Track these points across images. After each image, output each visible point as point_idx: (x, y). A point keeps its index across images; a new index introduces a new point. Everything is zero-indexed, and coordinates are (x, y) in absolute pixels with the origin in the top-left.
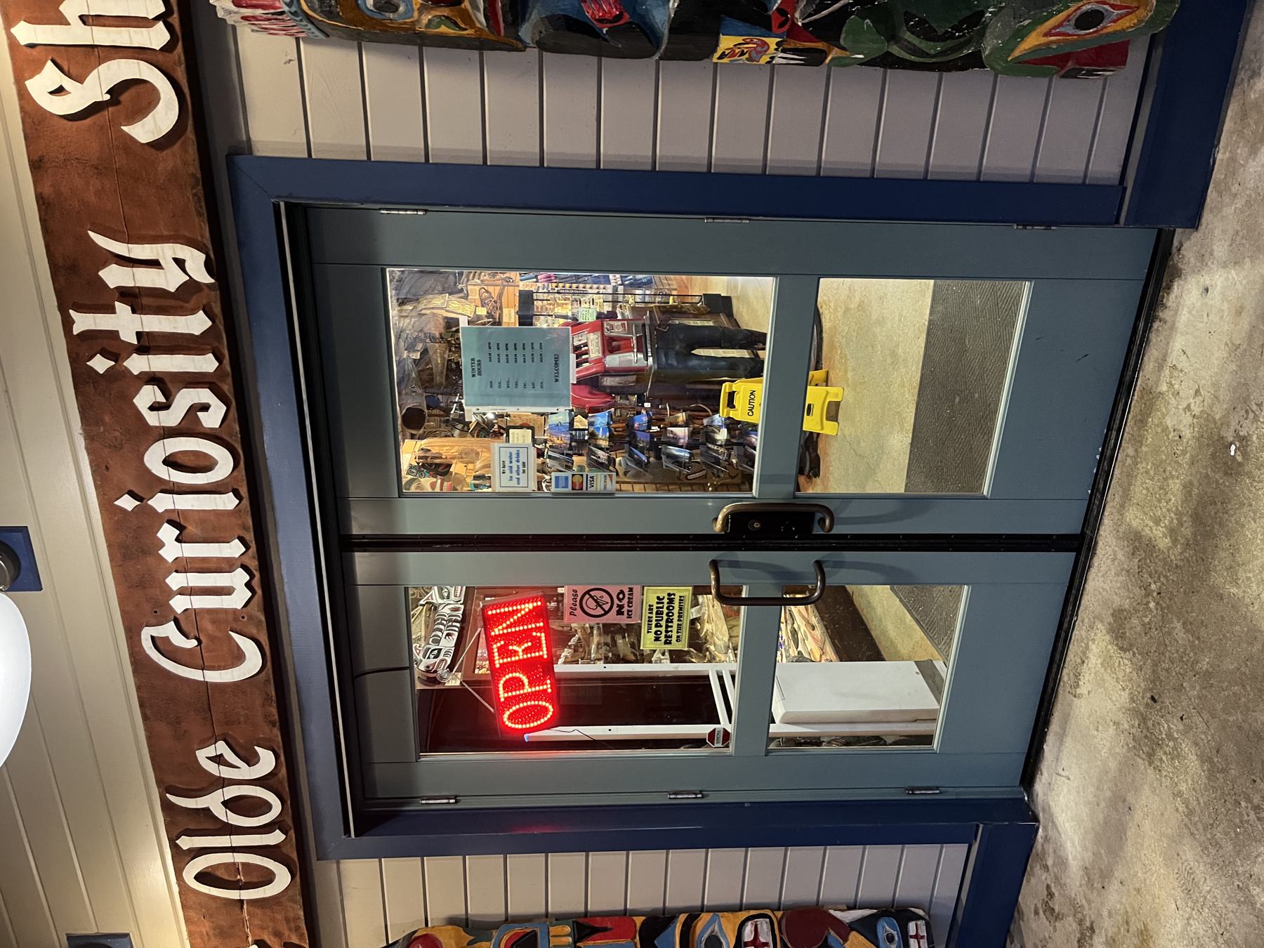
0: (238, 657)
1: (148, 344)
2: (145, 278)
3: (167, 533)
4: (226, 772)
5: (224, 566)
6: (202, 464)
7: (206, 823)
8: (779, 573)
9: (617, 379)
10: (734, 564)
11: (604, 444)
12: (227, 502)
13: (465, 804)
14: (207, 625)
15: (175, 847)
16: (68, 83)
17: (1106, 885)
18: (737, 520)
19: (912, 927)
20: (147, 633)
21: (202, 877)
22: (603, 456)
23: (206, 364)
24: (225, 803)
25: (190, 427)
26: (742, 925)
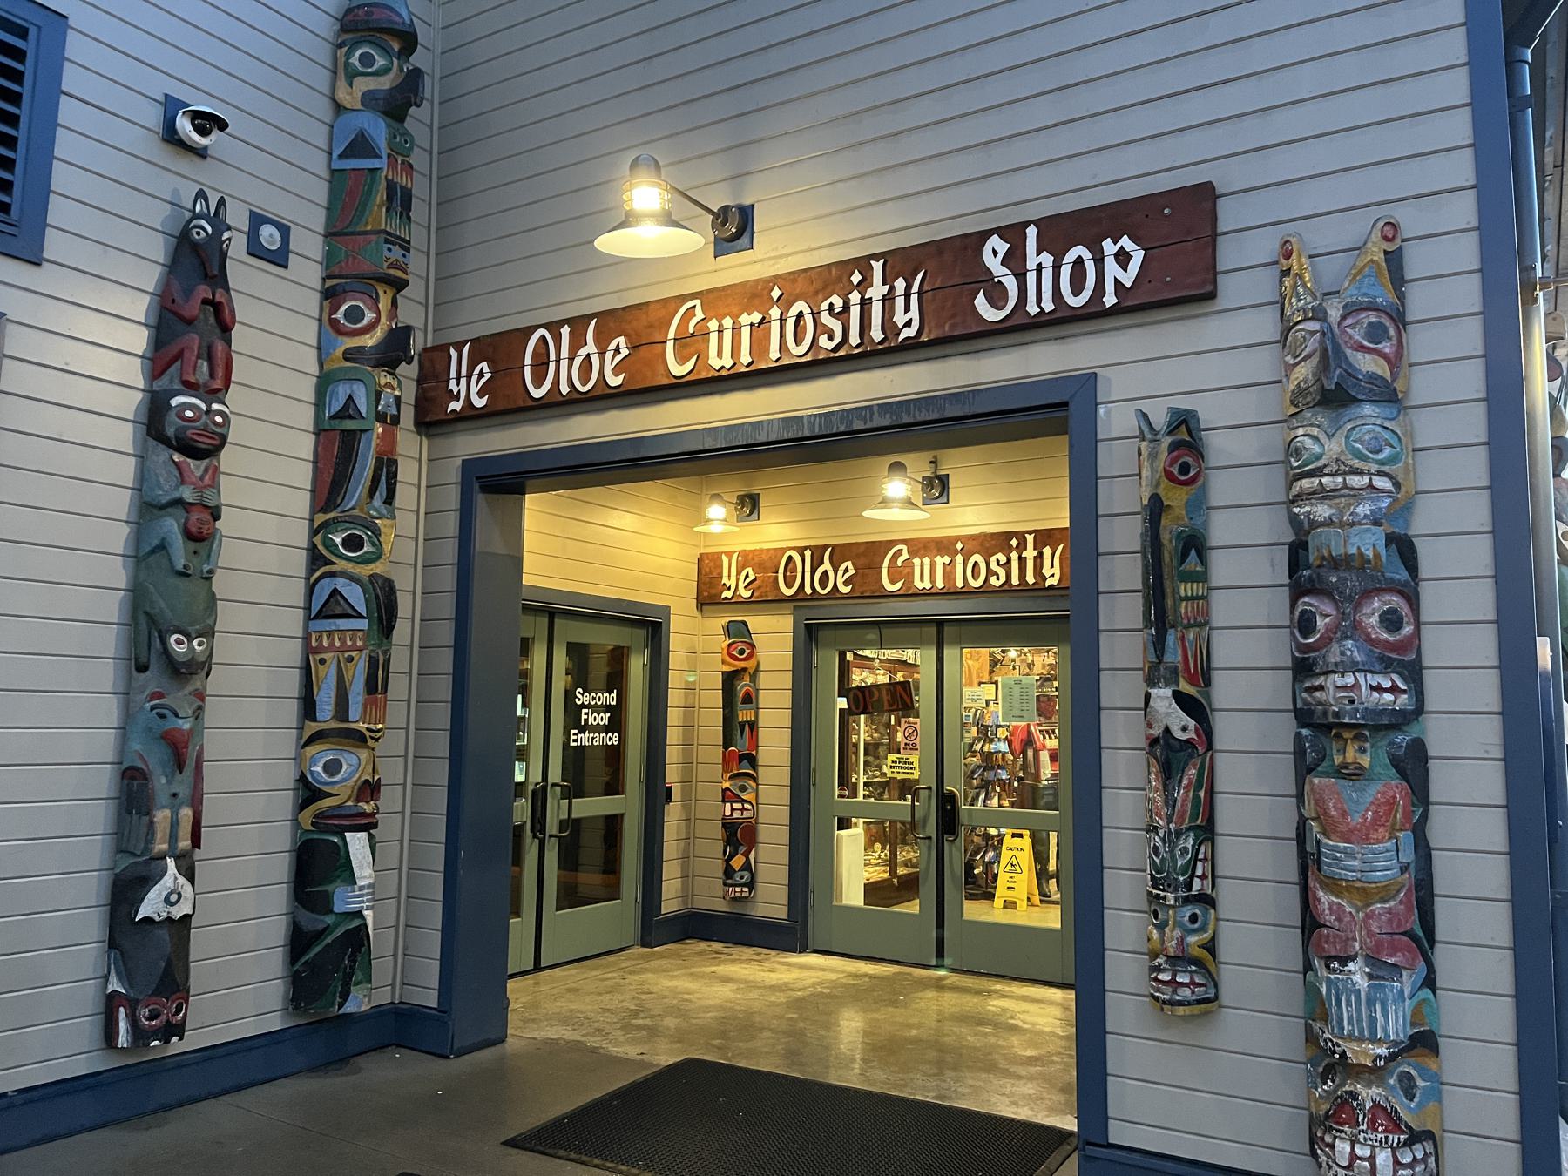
0: (893, 582)
1: (1022, 560)
2: (1047, 563)
3: (947, 560)
4: (840, 573)
5: (933, 580)
6: (975, 576)
7: (817, 562)
8: (925, 820)
9: (1032, 759)
10: (930, 797)
11: (986, 749)
12: (960, 584)
13: (814, 670)
14: (907, 570)
15: (806, 548)
16: (1000, 257)
18: (952, 798)
19: (746, 889)
20: (904, 548)
21: (790, 558)
22: (978, 747)
23: (1015, 581)
24: (826, 571)
25: (990, 572)
26: (751, 804)
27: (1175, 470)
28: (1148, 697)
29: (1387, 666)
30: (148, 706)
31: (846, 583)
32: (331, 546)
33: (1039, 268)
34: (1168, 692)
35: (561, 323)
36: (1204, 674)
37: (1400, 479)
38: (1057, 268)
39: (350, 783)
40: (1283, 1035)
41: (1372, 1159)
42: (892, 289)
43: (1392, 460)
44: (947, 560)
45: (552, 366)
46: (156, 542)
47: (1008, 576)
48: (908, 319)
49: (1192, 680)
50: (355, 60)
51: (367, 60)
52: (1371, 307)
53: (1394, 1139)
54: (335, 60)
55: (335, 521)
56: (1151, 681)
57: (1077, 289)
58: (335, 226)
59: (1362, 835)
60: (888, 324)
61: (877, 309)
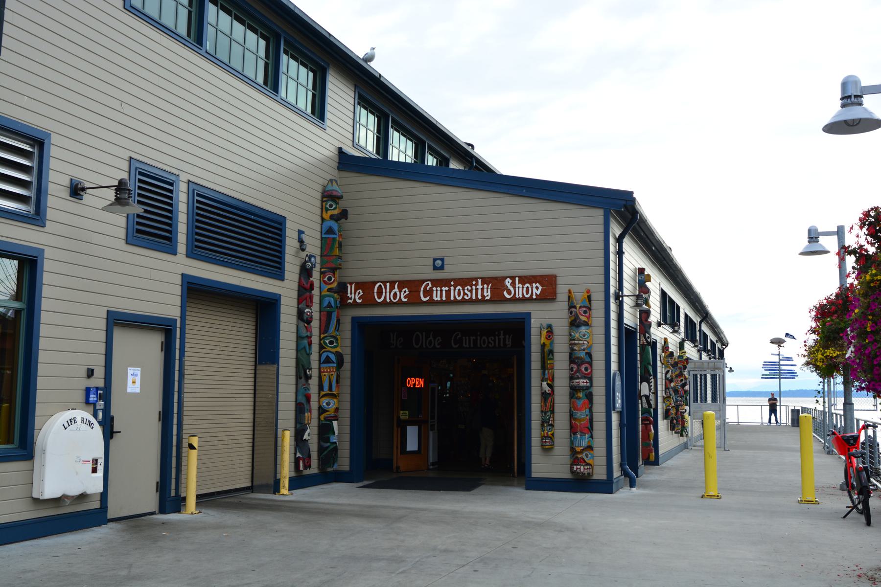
0: (425, 297)
1: (499, 340)
2: (507, 340)
3: (447, 289)
4: (402, 293)
5: (441, 296)
6: (459, 295)
12: (452, 298)
17: (863, 579)
20: (430, 282)
23: (474, 298)
25: (465, 294)
27: (547, 337)
28: (541, 384)
29: (585, 378)
30: (303, 387)
31: (405, 297)
32: (325, 343)
33: (519, 287)
34: (546, 383)
35: (387, 282)
36: (552, 380)
37: (589, 341)
38: (523, 288)
39: (333, 408)
40: (567, 451)
41: (580, 468)
42: (483, 287)
43: (587, 338)
44: (447, 289)
45: (384, 294)
46: (303, 347)
47: (495, 343)
48: (488, 294)
49: (550, 381)
50: (328, 206)
51: (331, 206)
52: (584, 307)
53: (584, 464)
54: (322, 206)
55: (326, 336)
56: (543, 380)
57: (527, 293)
59: (581, 410)
60: (482, 295)
61: (480, 291)
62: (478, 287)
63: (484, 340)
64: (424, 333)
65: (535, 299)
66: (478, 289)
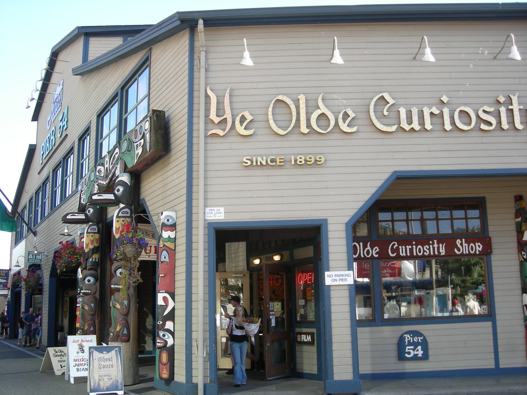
0: (393, 253)
1: (434, 248)
2: (441, 248)
3: (410, 247)
4: (374, 250)
5: (406, 253)
6: (420, 252)
16: (459, 243)
23: (432, 254)
25: (424, 251)
31: (376, 254)
44: (410, 247)
58: (428, 293)
62: (434, 246)
63: (420, 249)
64: (361, 244)
65: (478, 254)
66: (434, 247)
